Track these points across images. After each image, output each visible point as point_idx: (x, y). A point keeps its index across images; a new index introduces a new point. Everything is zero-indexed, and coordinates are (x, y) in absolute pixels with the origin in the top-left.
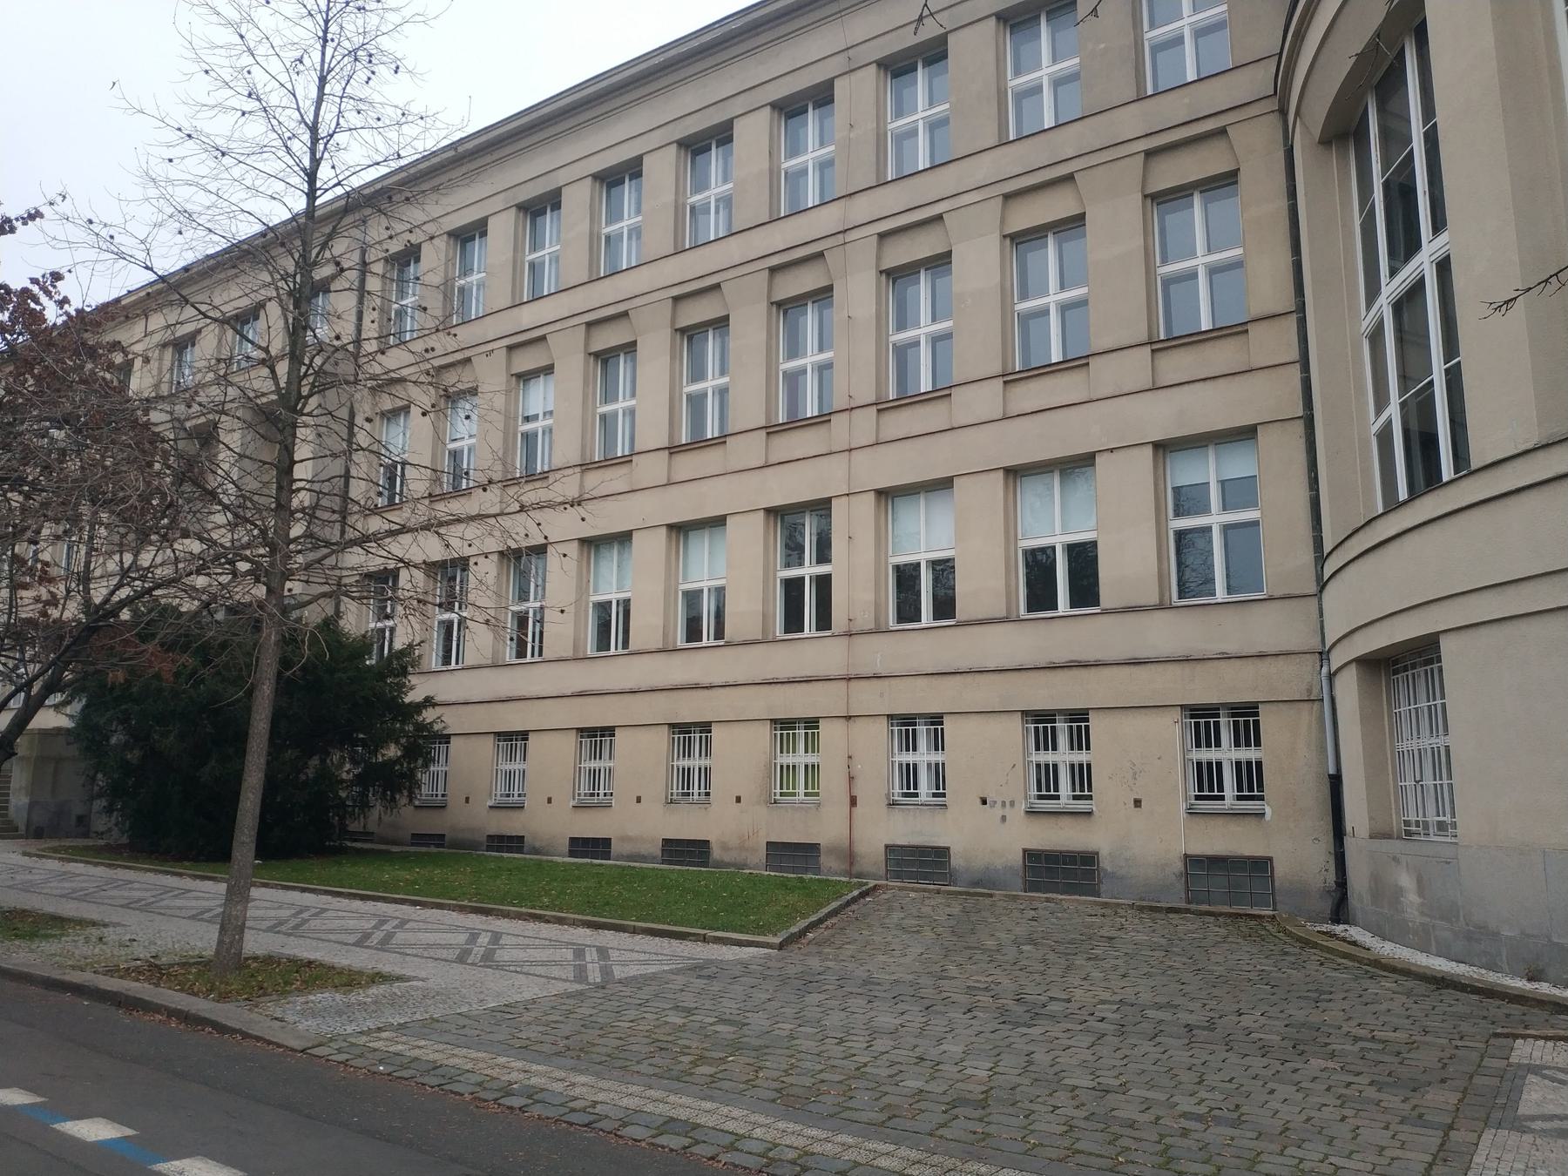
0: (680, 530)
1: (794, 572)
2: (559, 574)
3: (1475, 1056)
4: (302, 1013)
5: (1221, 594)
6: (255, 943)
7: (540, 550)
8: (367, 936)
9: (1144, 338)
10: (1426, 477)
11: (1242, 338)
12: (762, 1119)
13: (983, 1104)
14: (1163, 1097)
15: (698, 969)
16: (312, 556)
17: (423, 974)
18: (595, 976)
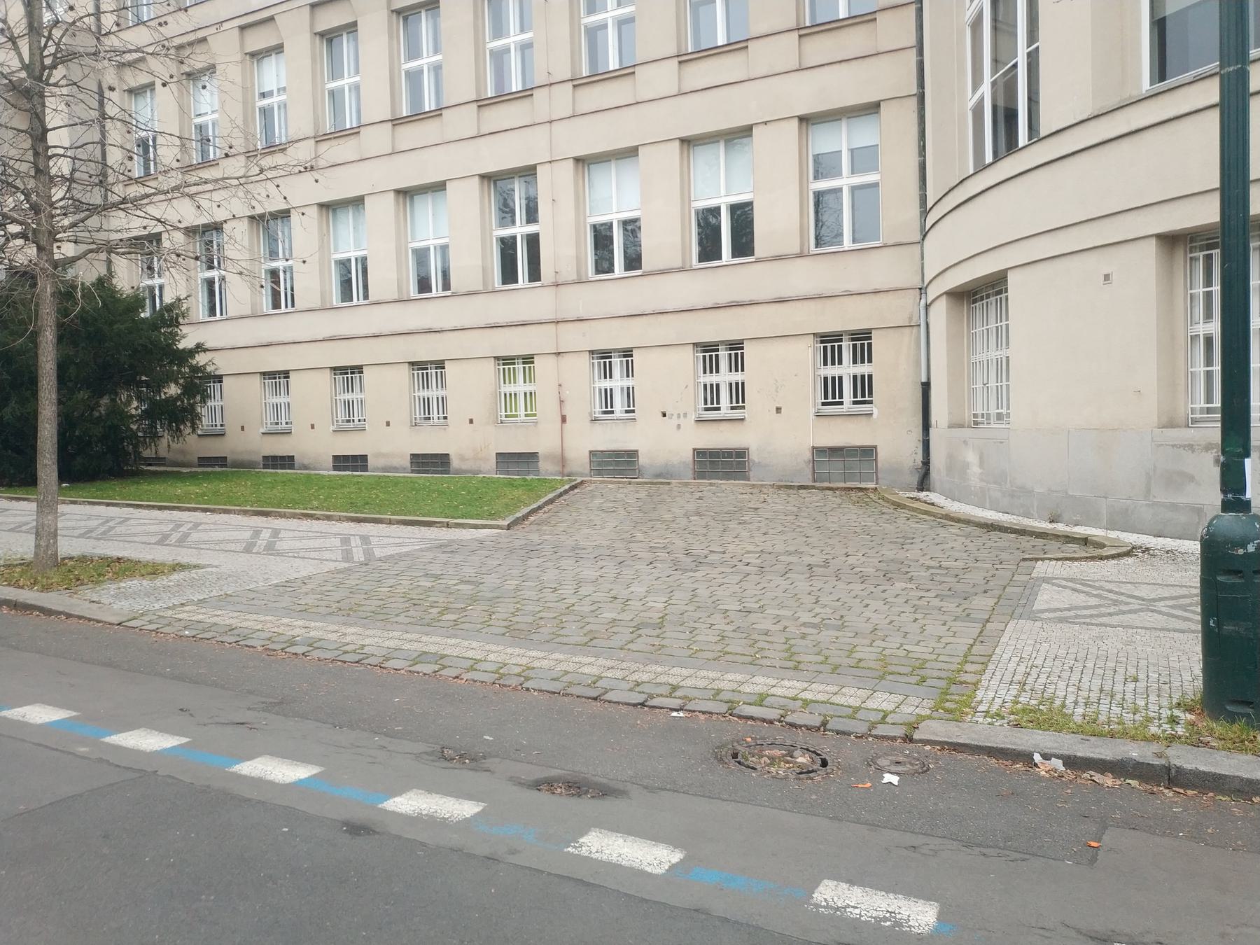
0: (406, 194)
1: (507, 232)
2: (303, 233)
3: (1009, 574)
4: (116, 596)
5: (847, 243)
6: (68, 547)
8: (165, 537)
9: (793, 25)
10: (1007, 143)
11: (871, 25)
12: (494, 648)
13: (660, 626)
14: (790, 614)
15: (442, 547)
16: (78, 217)
17: (216, 563)
18: (359, 555)
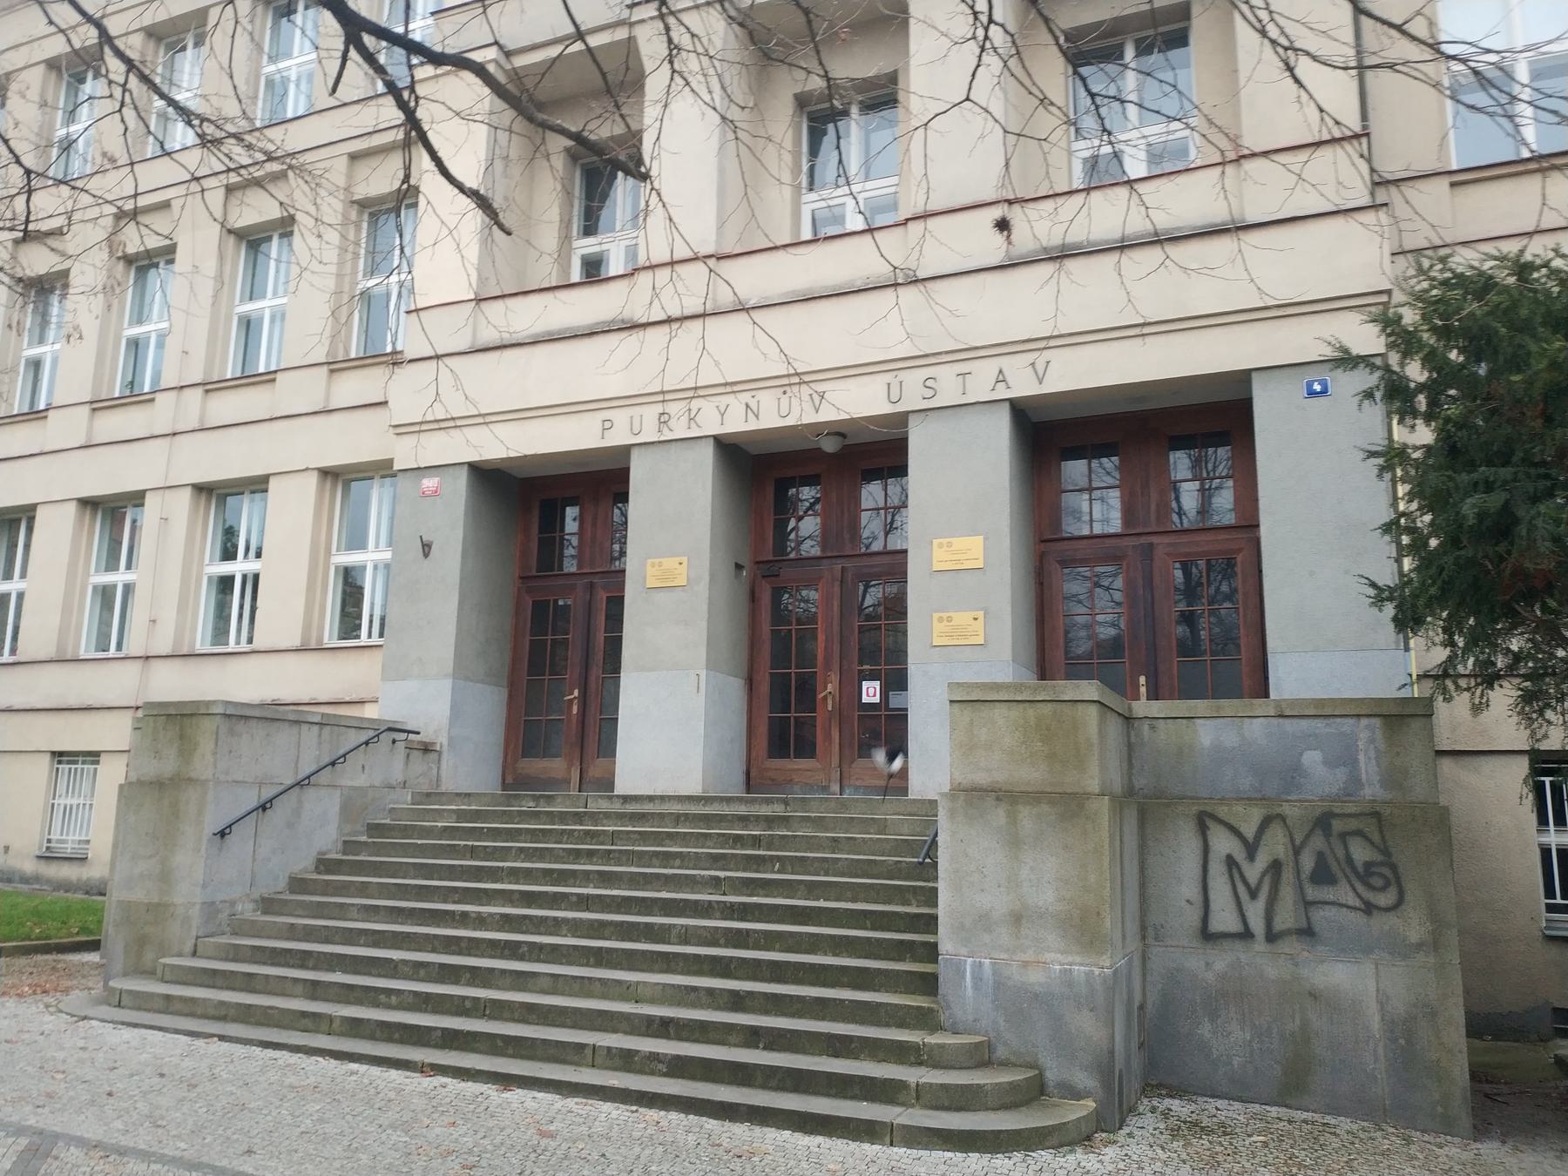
7: (137, 498)
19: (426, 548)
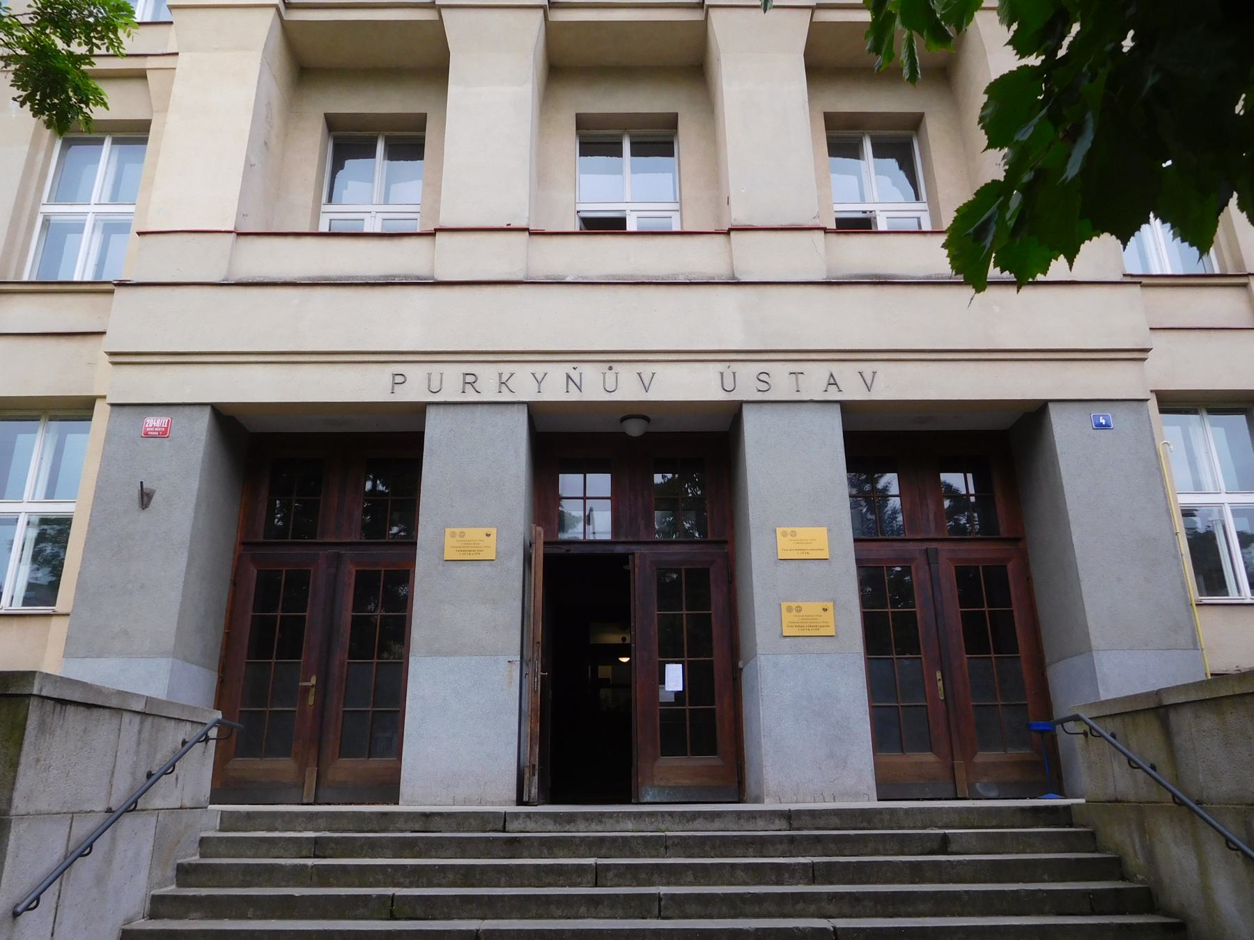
19: (145, 498)
